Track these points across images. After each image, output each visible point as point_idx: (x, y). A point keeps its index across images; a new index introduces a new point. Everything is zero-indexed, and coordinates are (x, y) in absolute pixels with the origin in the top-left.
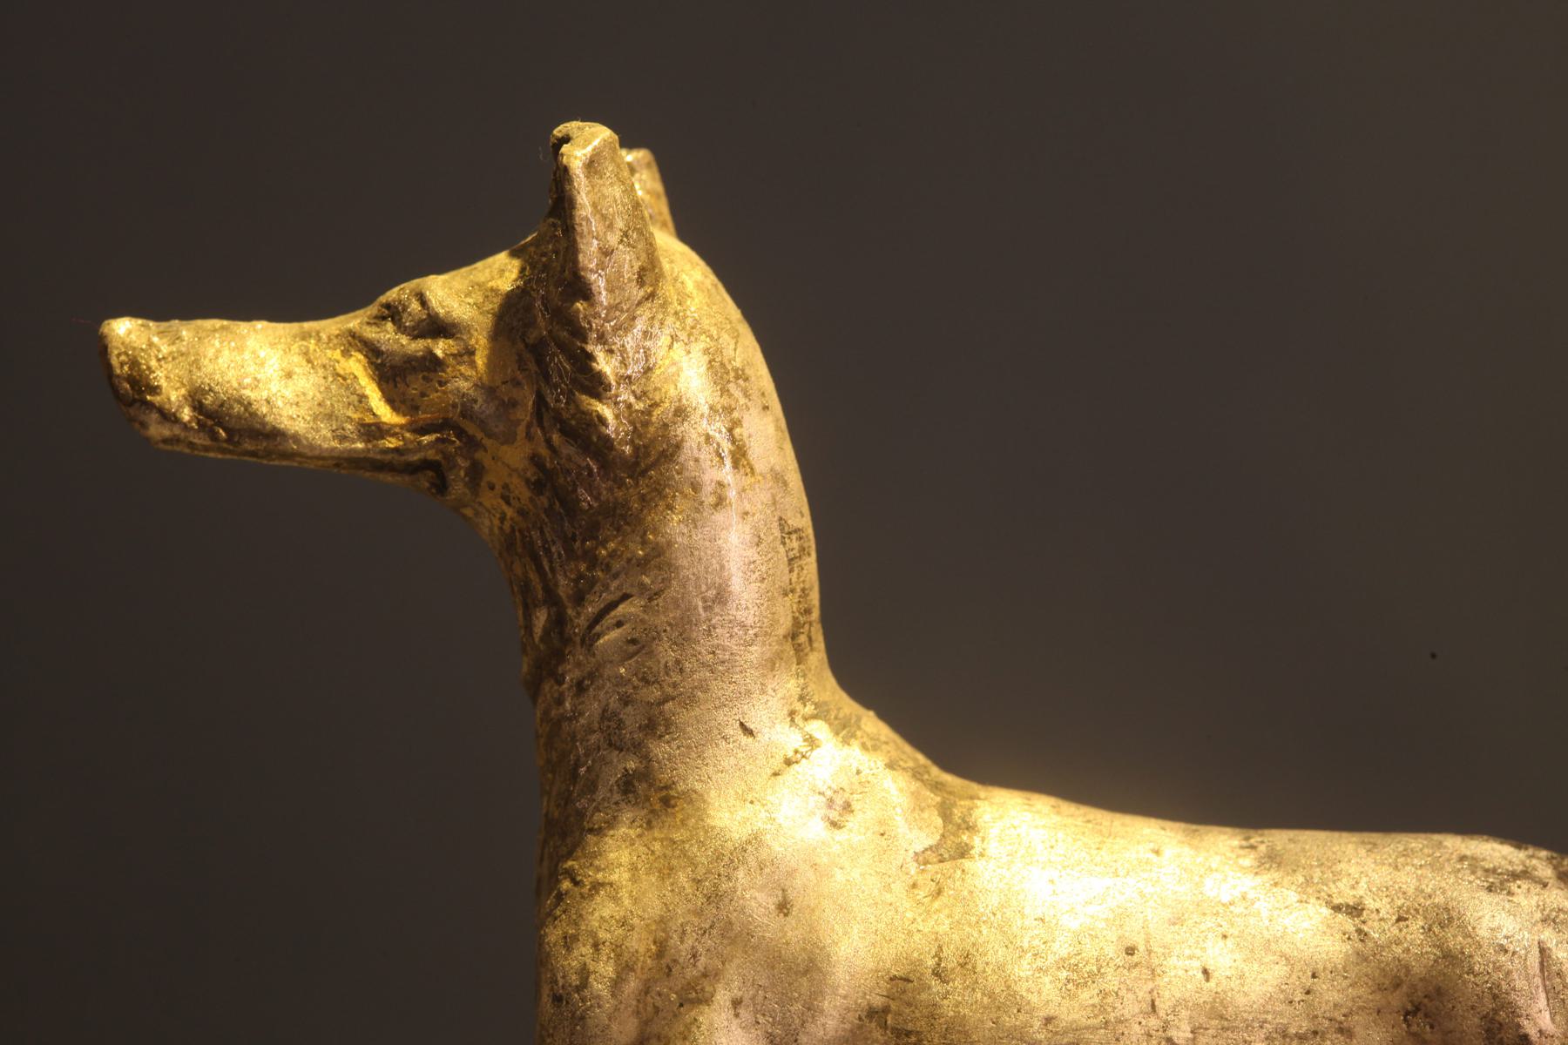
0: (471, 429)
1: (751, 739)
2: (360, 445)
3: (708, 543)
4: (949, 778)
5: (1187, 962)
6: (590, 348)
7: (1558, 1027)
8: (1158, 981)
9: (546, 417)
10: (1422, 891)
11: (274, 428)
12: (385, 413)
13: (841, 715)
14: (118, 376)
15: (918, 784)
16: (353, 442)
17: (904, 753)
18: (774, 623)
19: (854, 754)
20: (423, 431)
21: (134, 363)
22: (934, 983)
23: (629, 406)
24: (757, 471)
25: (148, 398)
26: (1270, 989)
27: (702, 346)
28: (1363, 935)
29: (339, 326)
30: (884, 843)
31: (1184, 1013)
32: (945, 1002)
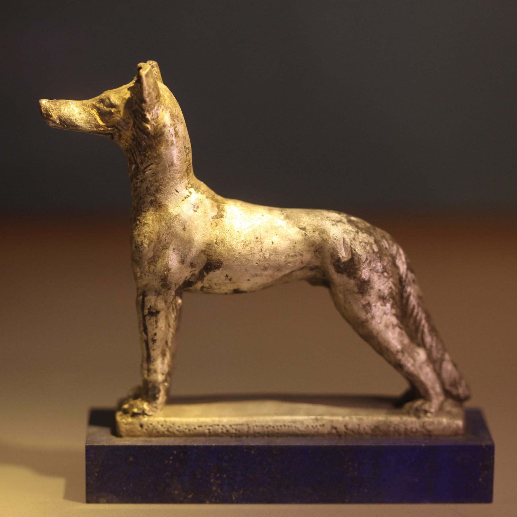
0: (119, 127)
1: (178, 193)
2: (95, 129)
3: (169, 153)
6: (145, 113)
7: (346, 255)
9: (136, 126)
11: (77, 125)
12: (101, 123)
13: (196, 186)
14: (43, 113)
15: (213, 201)
16: (94, 128)
19: (199, 196)
20: (109, 127)
21: (47, 110)
22: (215, 245)
23: (153, 125)
24: (180, 137)
25: (50, 118)
26: (286, 246)
27: (169, 111)
28: (306, 235)
29: (91, 103)
30: (205, 215)
31: (268, 251)
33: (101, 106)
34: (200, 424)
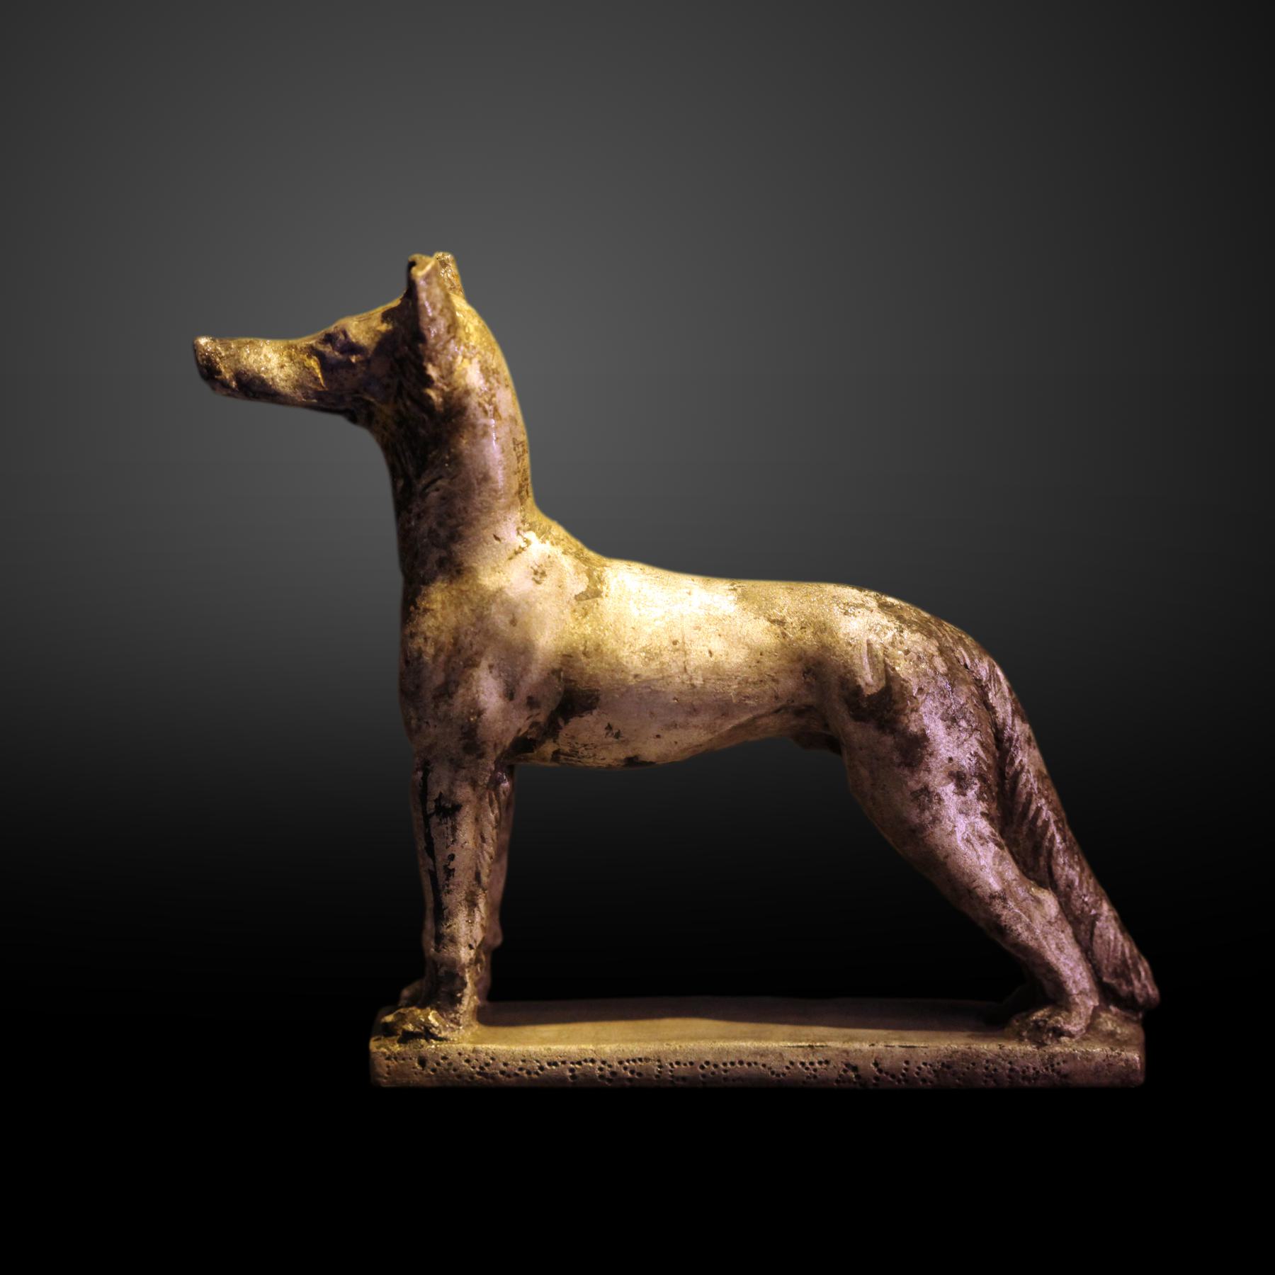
4: (591, 554)
5: (702, 648)
7: (875, 681)
8: (688, 657)
10: (813, 614)
17: (571, 543)
18: (510, 488)
19: (547, 548)
22: (583, 658)
28: (784, 635)
30: (561, 591)
32: (588, 667)
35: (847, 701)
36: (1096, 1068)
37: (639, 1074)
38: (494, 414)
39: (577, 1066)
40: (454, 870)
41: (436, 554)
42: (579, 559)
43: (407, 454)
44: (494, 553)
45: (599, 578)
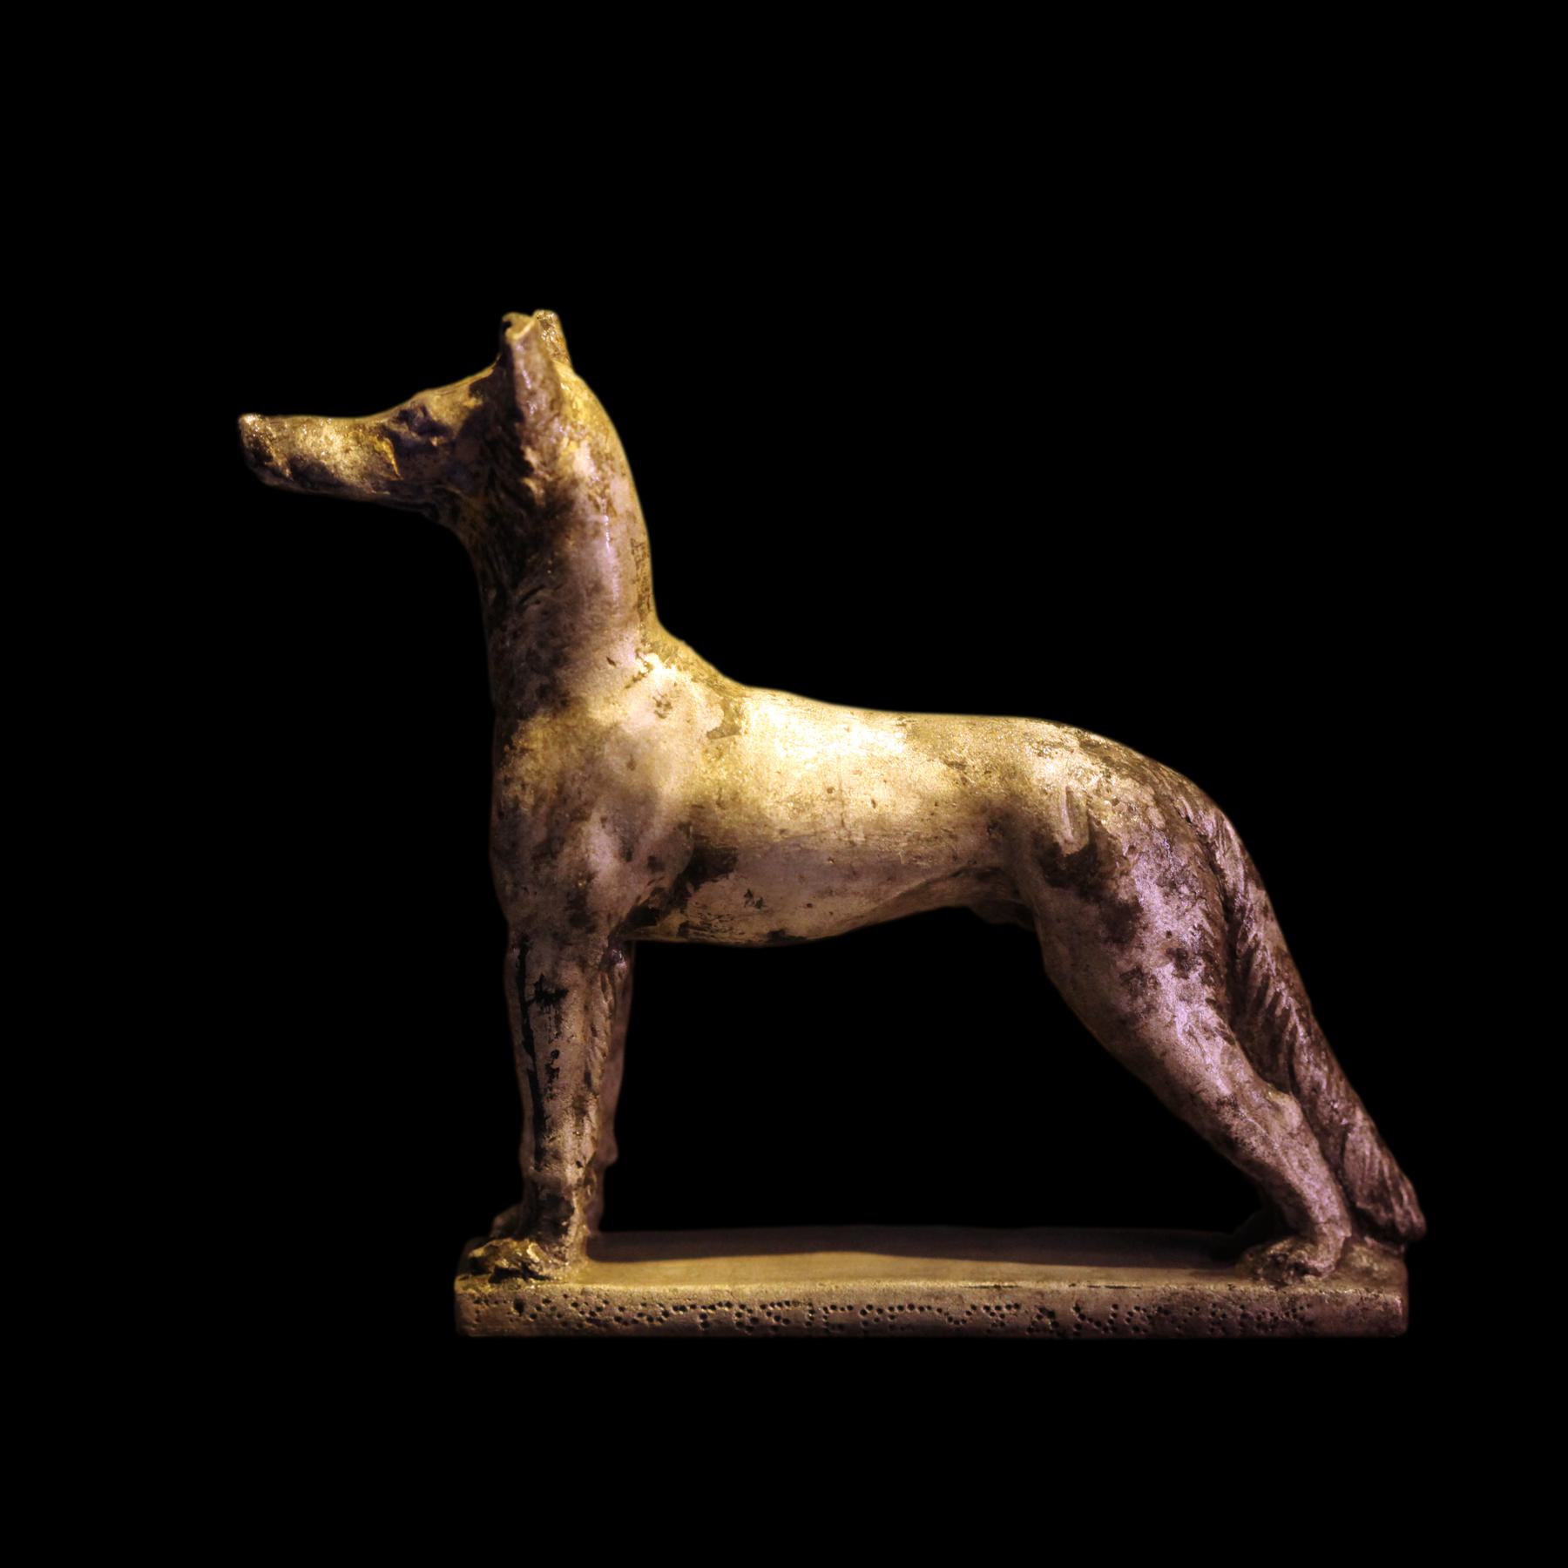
4: (727, 682)
5: (864, 796)
7: (1076, 838)
8: (846, 808)
14: (247, 450)
17: (702, 668)
18: (628, 600)
22: (716, 809)
28: (965, 781)
30: (690, 727)
32: (723, 821)
33: (403, 430)
34: (675, 1302)
35: (1041, 862)
36: (1348, 1314)
37: (786, 1321)
38: (607, 510)
39: (710, 1311)
40: (558, 1070)
41: (536, 682)
42: (712, 687)
43: (501, 558)
44: (608, 681)
45: (736, 711)
